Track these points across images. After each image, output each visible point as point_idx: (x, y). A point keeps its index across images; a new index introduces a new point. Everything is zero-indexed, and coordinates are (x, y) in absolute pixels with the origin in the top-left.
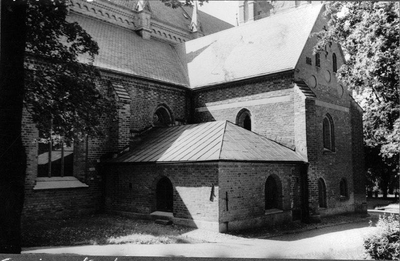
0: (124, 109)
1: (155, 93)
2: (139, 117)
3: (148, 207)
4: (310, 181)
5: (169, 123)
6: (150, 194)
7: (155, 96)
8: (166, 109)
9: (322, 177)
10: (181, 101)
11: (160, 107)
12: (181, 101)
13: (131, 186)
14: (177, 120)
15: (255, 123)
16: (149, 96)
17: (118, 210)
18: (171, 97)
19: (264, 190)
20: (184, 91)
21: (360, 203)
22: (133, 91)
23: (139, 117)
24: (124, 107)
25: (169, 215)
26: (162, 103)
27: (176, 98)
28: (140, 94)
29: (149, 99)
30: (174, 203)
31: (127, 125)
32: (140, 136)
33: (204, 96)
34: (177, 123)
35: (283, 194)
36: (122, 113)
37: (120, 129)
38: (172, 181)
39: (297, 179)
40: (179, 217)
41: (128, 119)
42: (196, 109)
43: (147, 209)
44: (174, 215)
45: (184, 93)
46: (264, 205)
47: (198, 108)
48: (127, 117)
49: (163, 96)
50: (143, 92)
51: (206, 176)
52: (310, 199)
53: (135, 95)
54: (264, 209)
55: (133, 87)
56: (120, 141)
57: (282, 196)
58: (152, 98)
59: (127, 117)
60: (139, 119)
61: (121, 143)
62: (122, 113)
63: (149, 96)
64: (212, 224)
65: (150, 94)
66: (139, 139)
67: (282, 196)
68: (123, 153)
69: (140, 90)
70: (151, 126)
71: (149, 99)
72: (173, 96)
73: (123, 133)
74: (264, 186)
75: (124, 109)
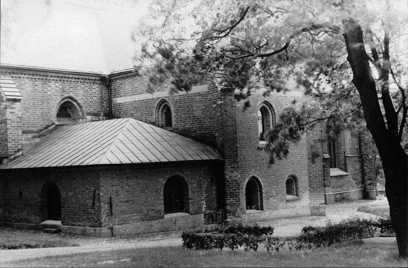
0: (14, 108)
1: (57, 85)
2: (37, 115)
3: (39, 216)
4: (229, 181)
5: (79, 119)
6: (39, 202)
7: (58, 89)
8: (74, 103)
9: (255, 175)
10: (94, 91)
11: (66, 100)
12: (94, 91)
13: (21, 193)
14: (88, 114)
15: (175, 117)
16: (49, 89)
17: (9, 221)
18: (79, 88)
19: (162, 193)
20: (97, 78)
21: (317, 203)
22: (27, 85)
23: (37, 115)
24: (13, 106)
25: (58, 223)
26: (67, 95)
27: (86, 88)
28: (36, 88)
29: (49, 93)
30: (62, 211)
31: (17, 127)
32: (39, 137)
33: (121, 84)
34: (89, 118)
35: (190, 197)
36: (11, 113)
37: (9, 132)
38: (59, 187)
39: (104, 174)
40: (67, 225)
41: (18, 119)
42: (114, 99)
43: (38, 218)
44: (63, 222)
45: (98, 80)
46: (62, 193)
47: (117, 99)
48: (18, 117)
49: (68, 87)
50: (40, 86)
51: (89, 182)
52: (229, 201)
53: (30, 89)
54: (163, 213)
55: (27, 80)
56: (9, 145)
57: (189, 199)
58: (53, 91)
59: (18, 117)
60: (36, 116)
61: (11, 147)
62: (11, 113)
63: (49, 89)
64: (95, 230)
65: (51, 87)
66: (38, 140)
67: (189, 199)
68: (15, 158)
69: (36, 83)
70: (54, 124)
71: (49, 93)
72: (82, 86)
73: (13, 136)
74: (163, 188)
75: (14, 108)
